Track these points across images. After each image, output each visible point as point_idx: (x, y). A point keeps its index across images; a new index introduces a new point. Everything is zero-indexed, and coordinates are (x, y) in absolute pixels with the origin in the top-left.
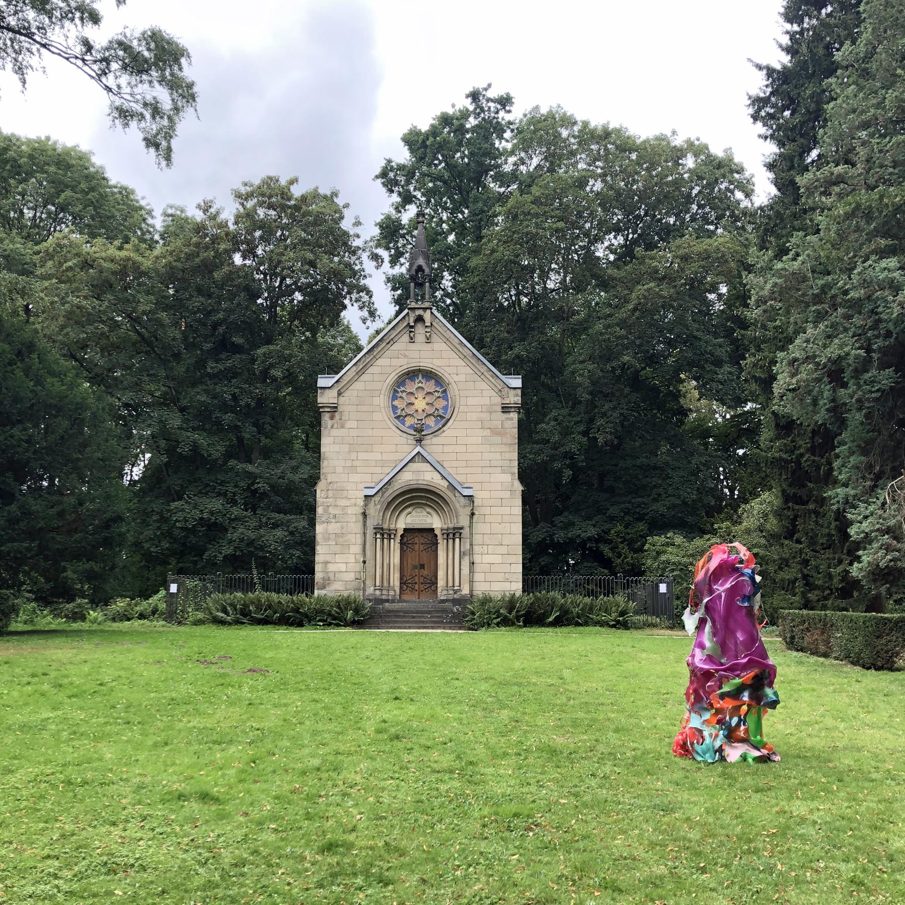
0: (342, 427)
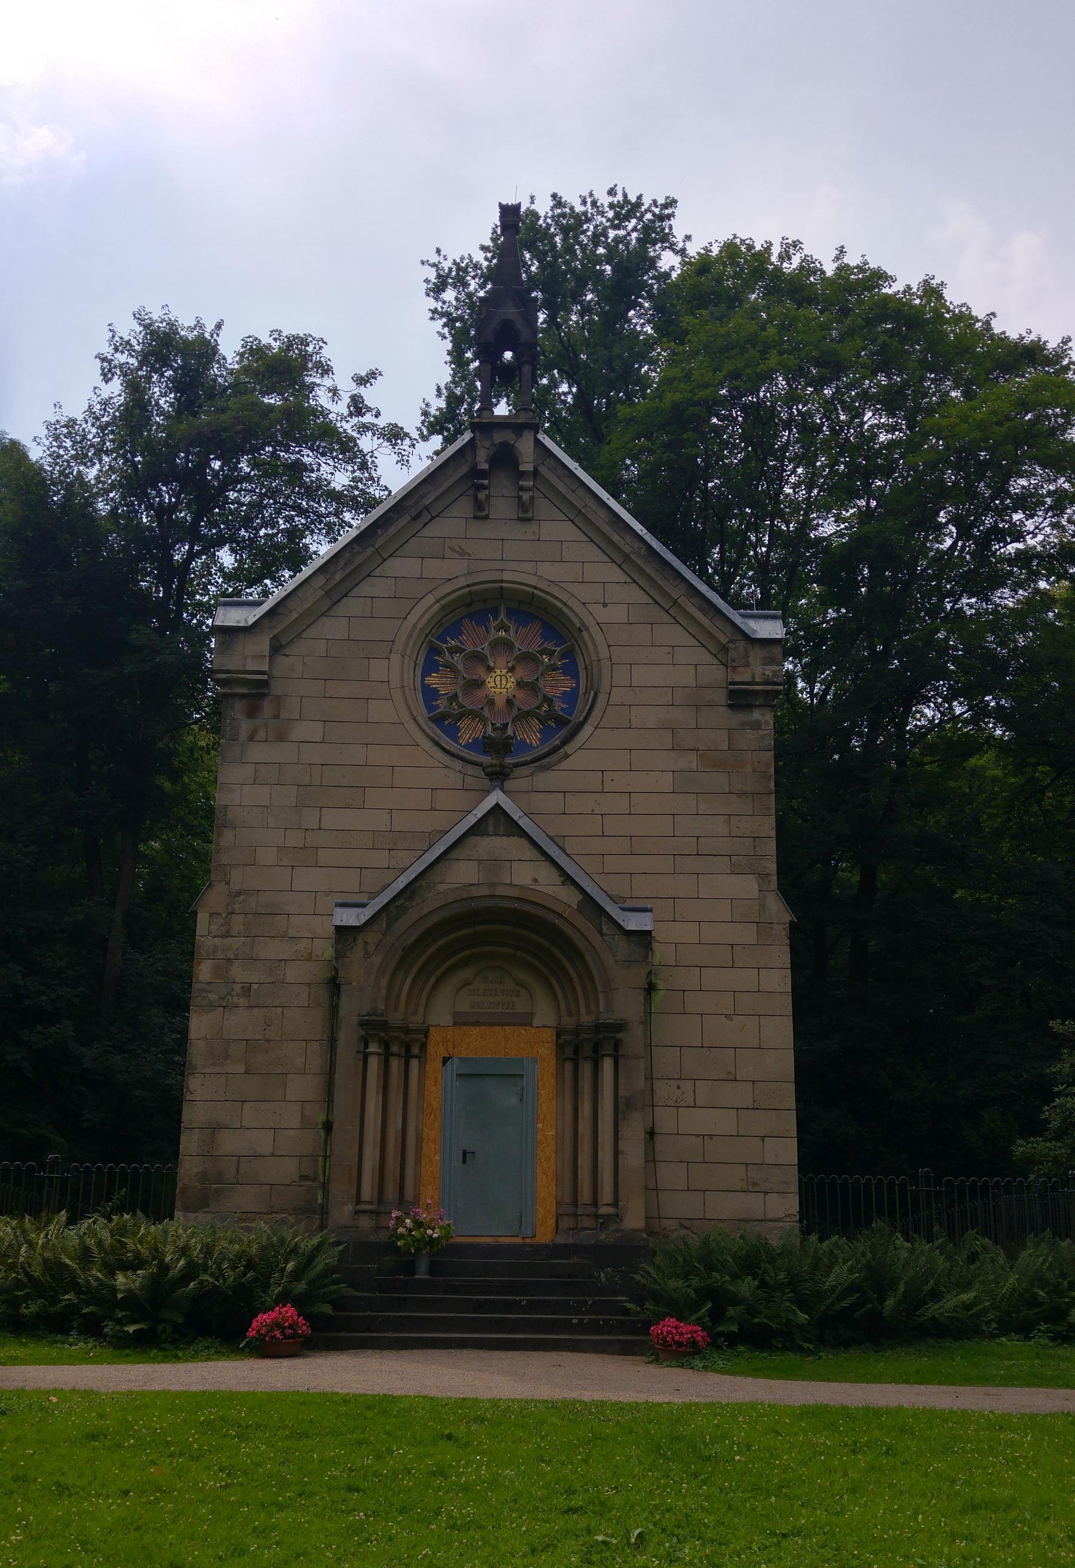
0: (281, 737)
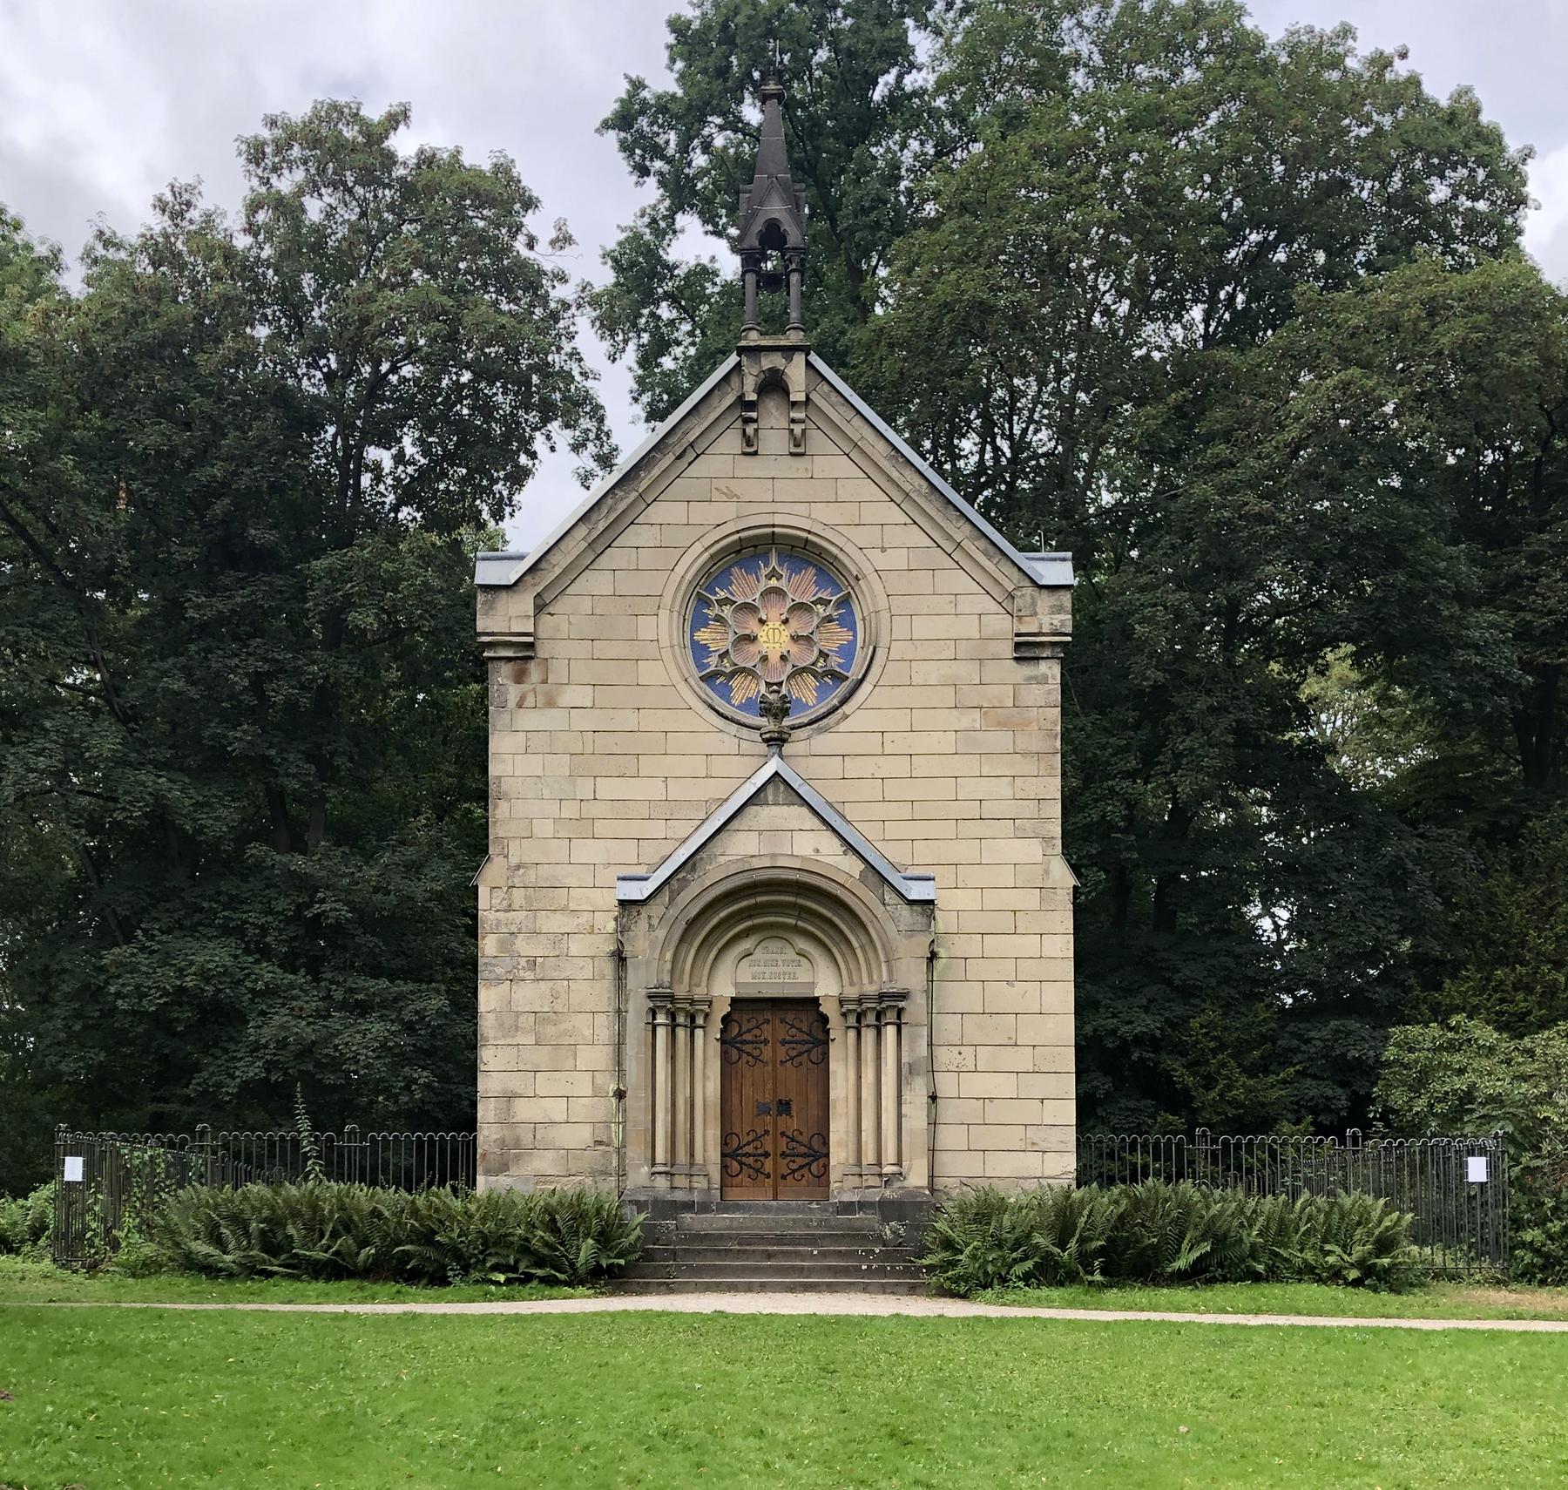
0: (550, 704)
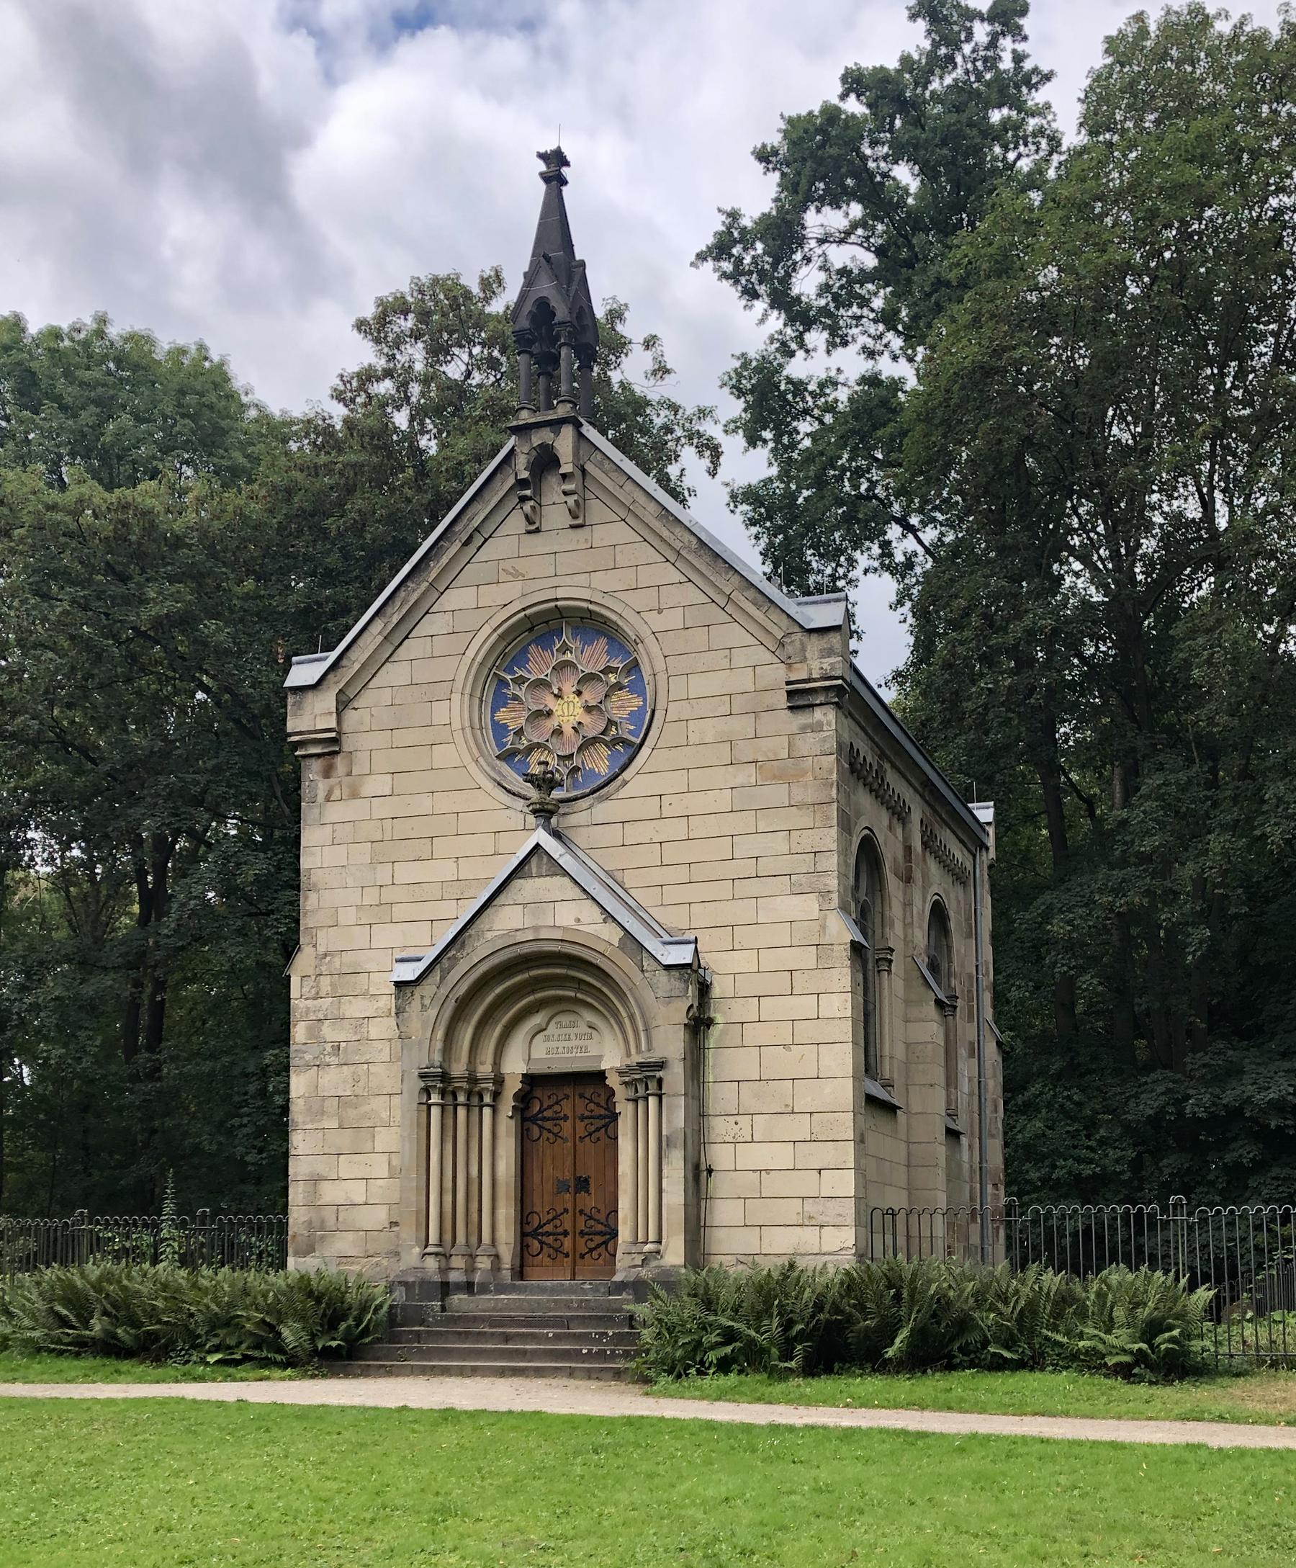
0: (354, 795)
